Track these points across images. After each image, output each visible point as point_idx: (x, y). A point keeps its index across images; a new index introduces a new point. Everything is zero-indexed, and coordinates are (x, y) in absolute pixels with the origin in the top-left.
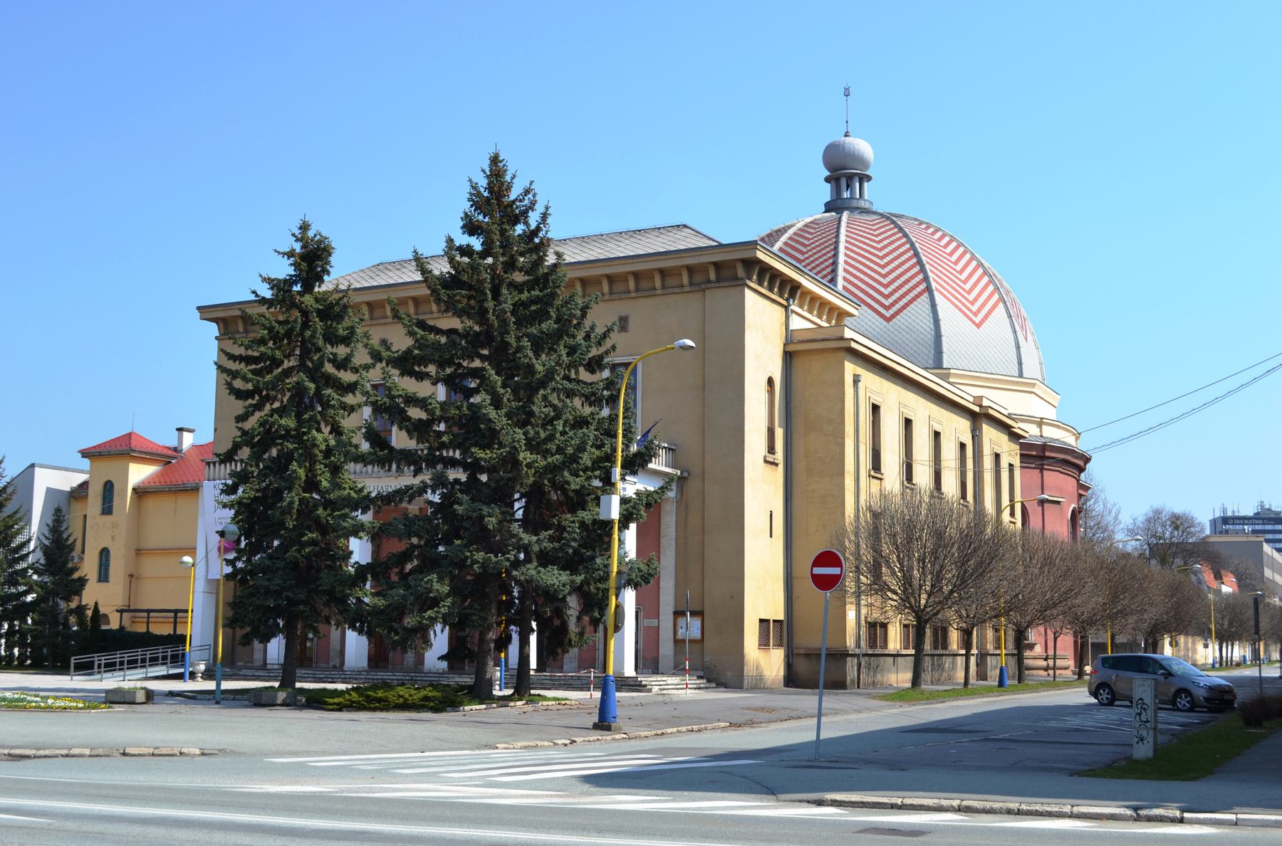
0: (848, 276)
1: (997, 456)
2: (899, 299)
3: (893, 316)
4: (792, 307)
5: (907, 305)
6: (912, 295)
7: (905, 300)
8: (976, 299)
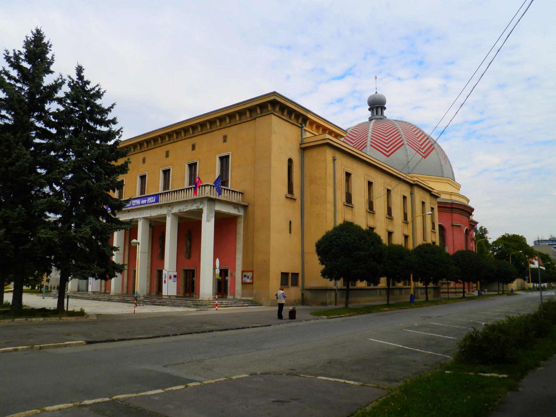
0: (373, 141)
1: (423, 203)
2: (392, 148)
3: (390, 155)
4: (305, 128)
5: (395, 150)
6: (397, 147)
7: (395, 149)
8: (424, 148)
